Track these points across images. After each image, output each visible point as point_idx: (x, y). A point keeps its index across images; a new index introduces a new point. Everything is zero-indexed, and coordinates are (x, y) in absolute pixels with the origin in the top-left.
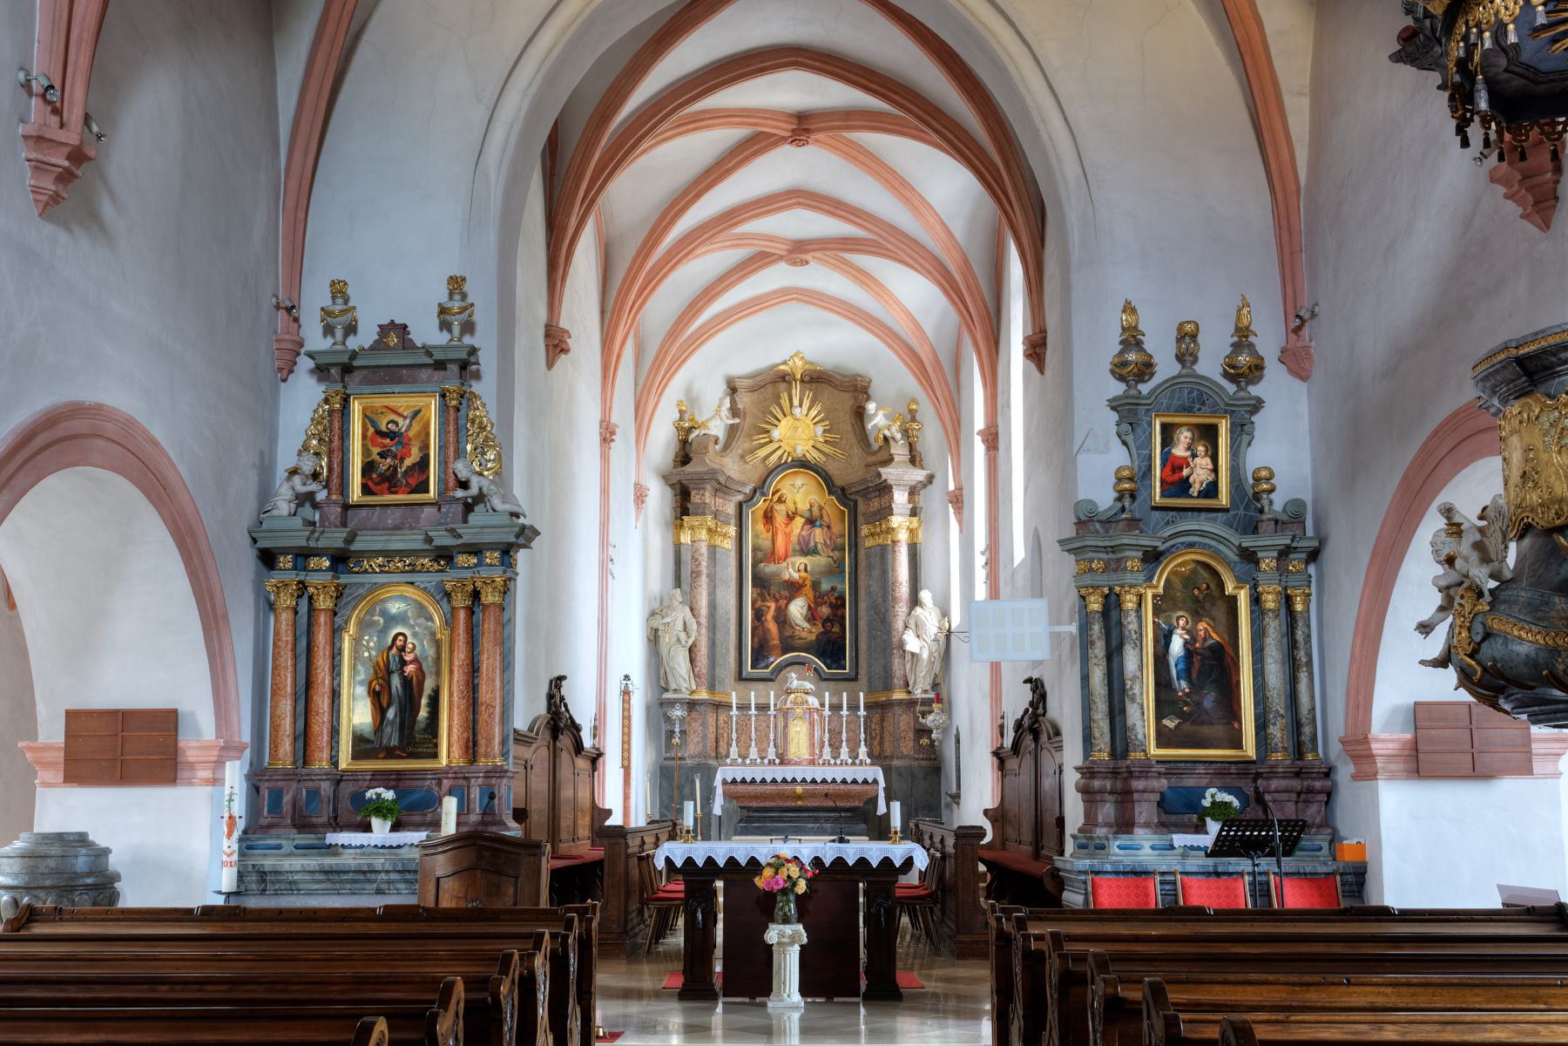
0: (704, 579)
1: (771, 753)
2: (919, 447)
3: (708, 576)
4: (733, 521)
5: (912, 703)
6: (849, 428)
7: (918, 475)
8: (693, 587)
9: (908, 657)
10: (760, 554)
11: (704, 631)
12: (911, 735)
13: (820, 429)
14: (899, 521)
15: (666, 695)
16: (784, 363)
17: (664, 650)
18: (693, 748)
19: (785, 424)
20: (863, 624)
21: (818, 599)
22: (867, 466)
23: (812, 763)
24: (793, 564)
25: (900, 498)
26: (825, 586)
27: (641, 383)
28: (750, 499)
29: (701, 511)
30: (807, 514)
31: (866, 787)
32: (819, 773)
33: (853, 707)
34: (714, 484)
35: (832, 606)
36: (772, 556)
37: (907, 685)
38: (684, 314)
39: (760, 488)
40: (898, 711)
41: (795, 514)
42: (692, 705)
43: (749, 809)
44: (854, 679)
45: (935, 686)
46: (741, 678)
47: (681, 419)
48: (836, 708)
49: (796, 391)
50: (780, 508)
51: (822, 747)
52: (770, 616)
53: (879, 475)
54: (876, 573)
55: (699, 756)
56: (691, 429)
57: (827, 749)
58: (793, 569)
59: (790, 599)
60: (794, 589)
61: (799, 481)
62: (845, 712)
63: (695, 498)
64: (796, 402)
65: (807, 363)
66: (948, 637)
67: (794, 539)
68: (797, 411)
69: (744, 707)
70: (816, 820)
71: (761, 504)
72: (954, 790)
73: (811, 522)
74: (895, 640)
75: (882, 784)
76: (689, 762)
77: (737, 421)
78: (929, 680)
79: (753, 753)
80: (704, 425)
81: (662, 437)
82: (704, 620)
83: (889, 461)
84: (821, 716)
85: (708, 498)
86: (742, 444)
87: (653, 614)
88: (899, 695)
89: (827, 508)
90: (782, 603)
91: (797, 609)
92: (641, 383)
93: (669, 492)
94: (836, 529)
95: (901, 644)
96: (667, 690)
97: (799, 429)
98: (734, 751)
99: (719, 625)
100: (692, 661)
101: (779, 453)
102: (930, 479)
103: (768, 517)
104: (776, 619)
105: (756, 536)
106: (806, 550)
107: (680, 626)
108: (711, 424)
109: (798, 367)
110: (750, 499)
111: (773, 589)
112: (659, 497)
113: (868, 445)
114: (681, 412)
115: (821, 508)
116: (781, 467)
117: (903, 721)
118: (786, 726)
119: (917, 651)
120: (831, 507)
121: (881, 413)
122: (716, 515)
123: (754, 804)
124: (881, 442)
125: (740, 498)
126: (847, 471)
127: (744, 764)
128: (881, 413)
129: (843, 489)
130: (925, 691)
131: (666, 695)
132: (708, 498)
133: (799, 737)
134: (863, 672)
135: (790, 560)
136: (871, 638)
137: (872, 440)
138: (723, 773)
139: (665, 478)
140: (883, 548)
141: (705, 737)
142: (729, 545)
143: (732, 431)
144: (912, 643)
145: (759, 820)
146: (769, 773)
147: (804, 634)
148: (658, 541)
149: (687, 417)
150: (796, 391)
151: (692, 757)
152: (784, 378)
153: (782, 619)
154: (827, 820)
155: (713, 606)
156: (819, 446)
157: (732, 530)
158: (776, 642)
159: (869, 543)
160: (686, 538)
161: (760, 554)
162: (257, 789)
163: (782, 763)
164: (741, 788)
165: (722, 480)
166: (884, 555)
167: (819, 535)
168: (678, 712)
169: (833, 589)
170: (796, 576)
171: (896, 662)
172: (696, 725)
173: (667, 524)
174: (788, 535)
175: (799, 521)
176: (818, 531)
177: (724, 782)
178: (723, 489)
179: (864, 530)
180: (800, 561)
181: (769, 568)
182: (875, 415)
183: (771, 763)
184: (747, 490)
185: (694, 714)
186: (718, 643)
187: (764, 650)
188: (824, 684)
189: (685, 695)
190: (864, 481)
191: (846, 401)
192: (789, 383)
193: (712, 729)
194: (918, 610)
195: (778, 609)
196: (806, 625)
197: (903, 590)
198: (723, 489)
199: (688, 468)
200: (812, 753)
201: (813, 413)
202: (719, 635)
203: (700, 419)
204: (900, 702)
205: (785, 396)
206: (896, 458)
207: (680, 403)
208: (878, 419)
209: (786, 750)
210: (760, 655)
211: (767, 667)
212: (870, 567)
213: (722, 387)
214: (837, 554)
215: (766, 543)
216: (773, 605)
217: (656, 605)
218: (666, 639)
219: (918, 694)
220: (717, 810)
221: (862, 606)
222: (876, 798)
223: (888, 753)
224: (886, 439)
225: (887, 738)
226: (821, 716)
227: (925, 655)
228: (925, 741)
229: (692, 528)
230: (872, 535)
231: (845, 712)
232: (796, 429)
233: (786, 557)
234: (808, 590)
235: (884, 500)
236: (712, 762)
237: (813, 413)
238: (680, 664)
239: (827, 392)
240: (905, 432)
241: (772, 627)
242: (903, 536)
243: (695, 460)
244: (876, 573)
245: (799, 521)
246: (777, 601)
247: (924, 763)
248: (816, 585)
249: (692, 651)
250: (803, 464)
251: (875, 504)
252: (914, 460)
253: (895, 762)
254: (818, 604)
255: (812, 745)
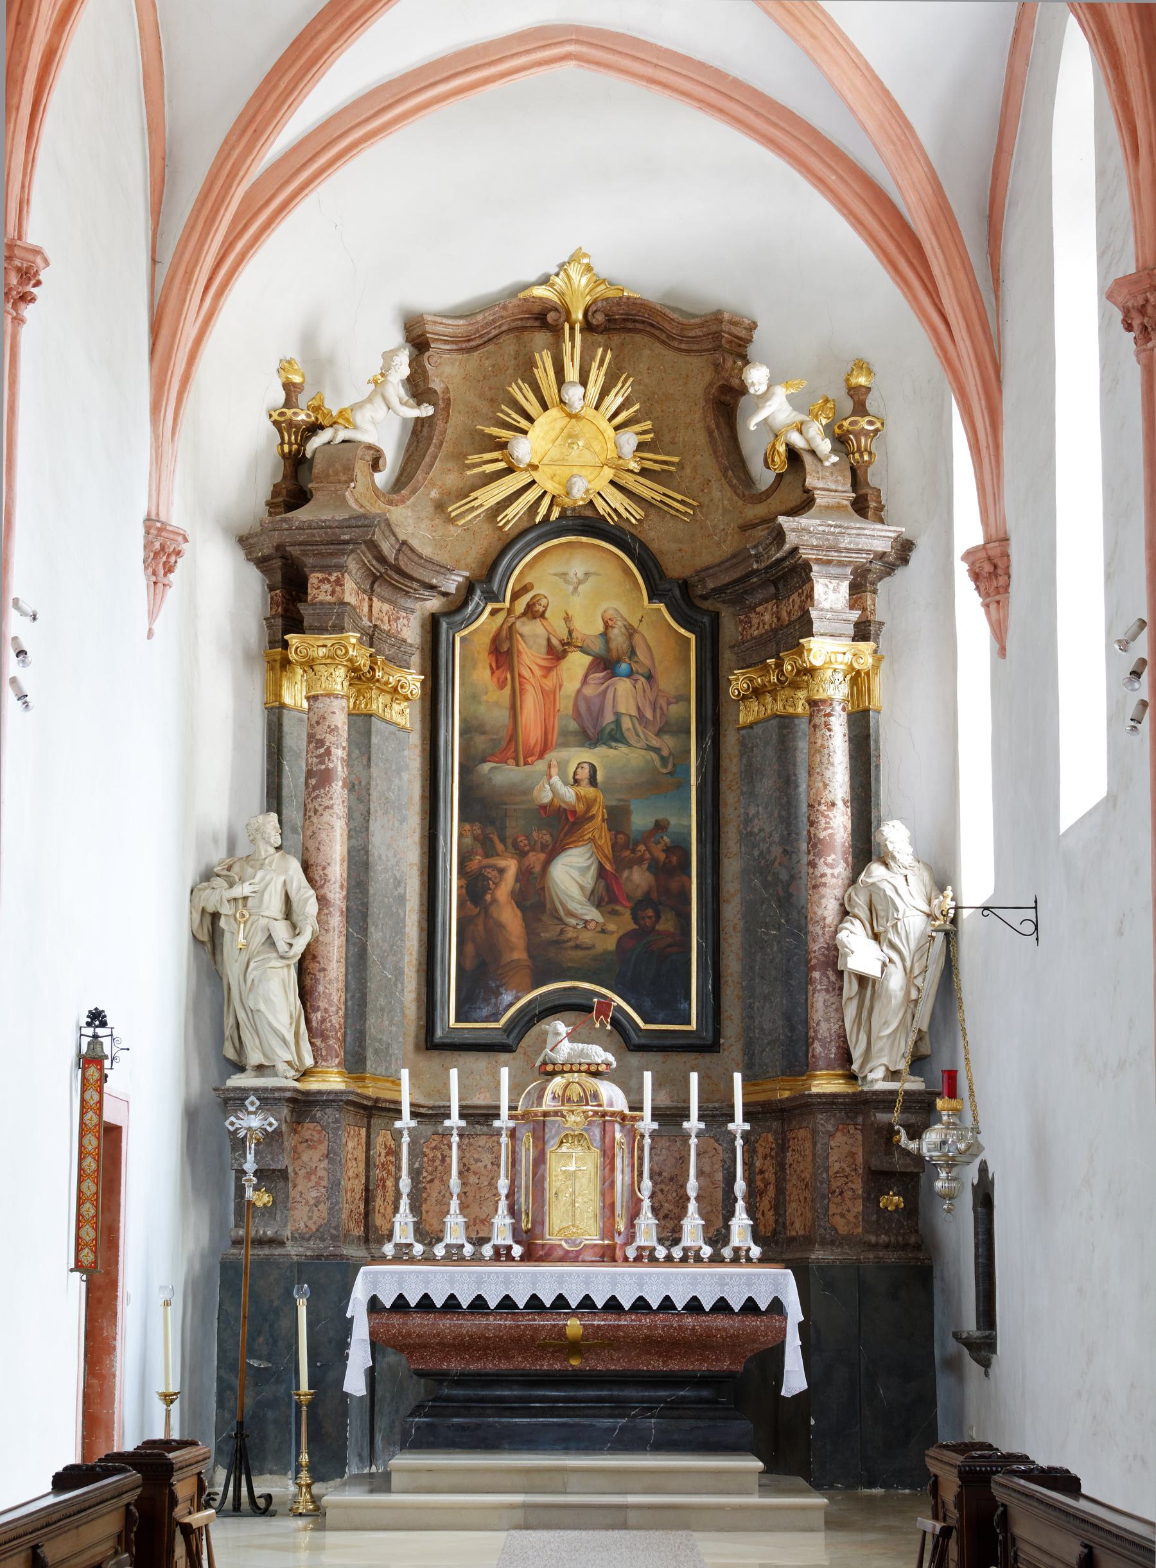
0: (338, 792)
1: (501, 1230)
2: (874, 478)
3: (351, 787)
4: (416, 659)
5: (860, 1106)
6: (701, 439)
7: (877, 538)
8: (310, 812)
9: (850, 988)
10: (480, 742)
11: (336, 921)
12: (858, 1185)
13: (629, 440)
14: (828, 650)
15: (237, 1081)
16: (545, 281)
17: (232, 968)
18: (305, 1211)
19: (547, 425)
20: (732, 912)
21: (623, 849)
22: (745, 528)
23: (608, 1255)
24: (562, 766)
25: (829, 594)
26: (640, 820)
27: (167, 258)
28: (458, 606)
29: (334, 620)
30: (598, 646)
31: (753, 1322)
32: (626, 1283)
33: (716, 1114)
34: (368, 558)
35: (656, 868)
36: (509, 747)
37: (847, 1058)
38: (278, 70)
39: (484, 582)
40: (824, 1122)
41: (568, 644)
42: (303, 1106)
43: (440, 1377)
44: (706, 1045)
45: (918, 1062)
46: (432, 1042)
47: (288, 403)
48: (670, 1117)
49: (573, 351)
50: (530, 629)
51: (634, 1213)
52: (504, 890)
53: (779, 535)
54: (766, 785)
55: (320, 1234)
56: (314, 428)
57: (647, 1222)
58: (557, 779)
59: (553, 852)
60: (563, 825)
61: (578, 565)
62: (693, 1124)
63: (319, 590)
64: (572, 372)
65: (599, 281)
66: (951, 936)
67: (565, 704)
68: (574, 393)
69: (430, 1115)
70: (619, 1407)
71: (484, 621)
72: (970, 1324)
73: (606, 664)
74: (817, 947)
75: (795, 1313)
76: (293, 1250)
77: (427, 411)
78: (905, 1046)
79: (455, 1228)
80: (344, 418)
81: (232, 444)
82: (336, 894)
83: (805, 504)
84: (633, 1135)
85: (350, 591)
86: (441, 475)
87: (208, 876)
88: (825, 1084)
89: (647, 632)
90: (535, 859)
91: (571, 874)
92: (167, 258)
93: (254, 578)
94: (667, 682)
95: (833, 955)
96: (241, 1069)
97: (577, 442)
98: (403, 1225)
99: (374, 909)
100: (306, 994)
101: (531, 496)
102: (904, 549)
103: (502, 652)
104: (519, 898)
105: (470, 698)
106: (595, 731)
107: (274, 906)
108: (362, 417)
109: (579, 294)
110: (458, 606)
111: (514, 828)
112: (220, 586)
113: (748, 480)
114: (289, 387)
115: (631, 632)
116: (537, 530)
117: (842, 1148)
118: (540, 1160)
119: (872, 969)
120: (657, 627)
121: (780, 394)
122: (371, 637)
123: (455, 1365)
124: (780, 461)
125: (434, 604)
126: (698, 542)
127: (428, 1259)
128: (780, 394)
129: (685, 586)
130: (894, 1075)
131: (237, 1081)
132: (350, 591)
133: (575, 1191)
134: (732, 1030)
135: (553, 756)
136: (754, 944)
137: (756, 466)
138: (375, 1282)
139: (245, 542)
140: (786, 723)
141: (334, 1187)
142: (405, 715)
143: (419, 436)
144: (861, 954)
145: (466, 1407)
146: (496, 1282)
147: (586, 937)
148: (224, 702)
149: (303, 399)
150: (573, 351)
151: (300, 1238)
152: (540, 319)
153: (534, 897)
154: (648, 1409)
155: (360, 864)
156: (629, 481)
157: (413, 681)
158: (519, 955)
159: (749, 713)
160: (294, 694)
161: (480, 742)
162: (108, 1273)
163: (529, 1256)
164: (418, 1323)
165: (387, 548)
166: (786, 740)
167: (624, 695)
168: (252, 1122)
169: (660, 826)
170: (569, 794)
171: (820, 1001)
172: (312, 1157)
173: (248, 658)
174: (549, 696)
175: (578, 662)
176: (623, 686)
177: (374, 1305)
178: (392, 574)
179: (738, 682)
180: (578, 757)
181: (502, 775)
182: (765, 397)
183: (502, 1255)
184: (452, 583)
185: (309, 1130)
186: (373, 956)
187: (489, 983)
188: (635, 1059)
189: (285, 1080)
190: (739, 556)
191: (694, 375)
192: (555, 330)
193: (354, 1168)
194: (876, 871)
195: (524, 875)
196: (593, 914)
197: (838, 824)
198: (392, 574)
199: (303, 515)
200: (608, 1230)
201: (614, 401)
202: (376, 935)
203: (333, 406)
204: (831, 1101)
205: (545, 360)
206: (821, 499)
207: (285, 366)
208: (775, 408)
209: (539, 1221)
210: (477, 988)
211: (495, 1017)
212: (750, 774)
213: (395, 337)
214: (668, 743)
215: (496, 714)
216: (511, 866)
217: (218, 855)
218: (237, 938)
219: (877, 1080)
220: (355, 1383)
221: (732, 867)
222: (778, 1352)
223: (797, 1228)
224: (793, 455)
225: (794, 1191)
226: (633, 1135)
227: (896, 981)
228: (893, 1201)
229: (310, 665)
230: (757, 693)
231: (693, 1124)
232: (572, 438)
233: (545, 748)
234: (597, 828)
235: (789, 608)
236: (353, 1251)
237: (614, 401)
238: (274, 1000)
239: (648, 351)
240: (841, 441)
241: (510, 918)
242: (836, 690)
243: (318, 496)
244: (766, 785)
245: (578, 662)
246: (521, 854)
247: (892, 1257)
248: (617, 817)
249: (306, 969)
250: (586, 523)
251: (765, 617)
252: (864, 504)
253: (819, 1255)
254: (621, 864)
255: (609, 1208)
